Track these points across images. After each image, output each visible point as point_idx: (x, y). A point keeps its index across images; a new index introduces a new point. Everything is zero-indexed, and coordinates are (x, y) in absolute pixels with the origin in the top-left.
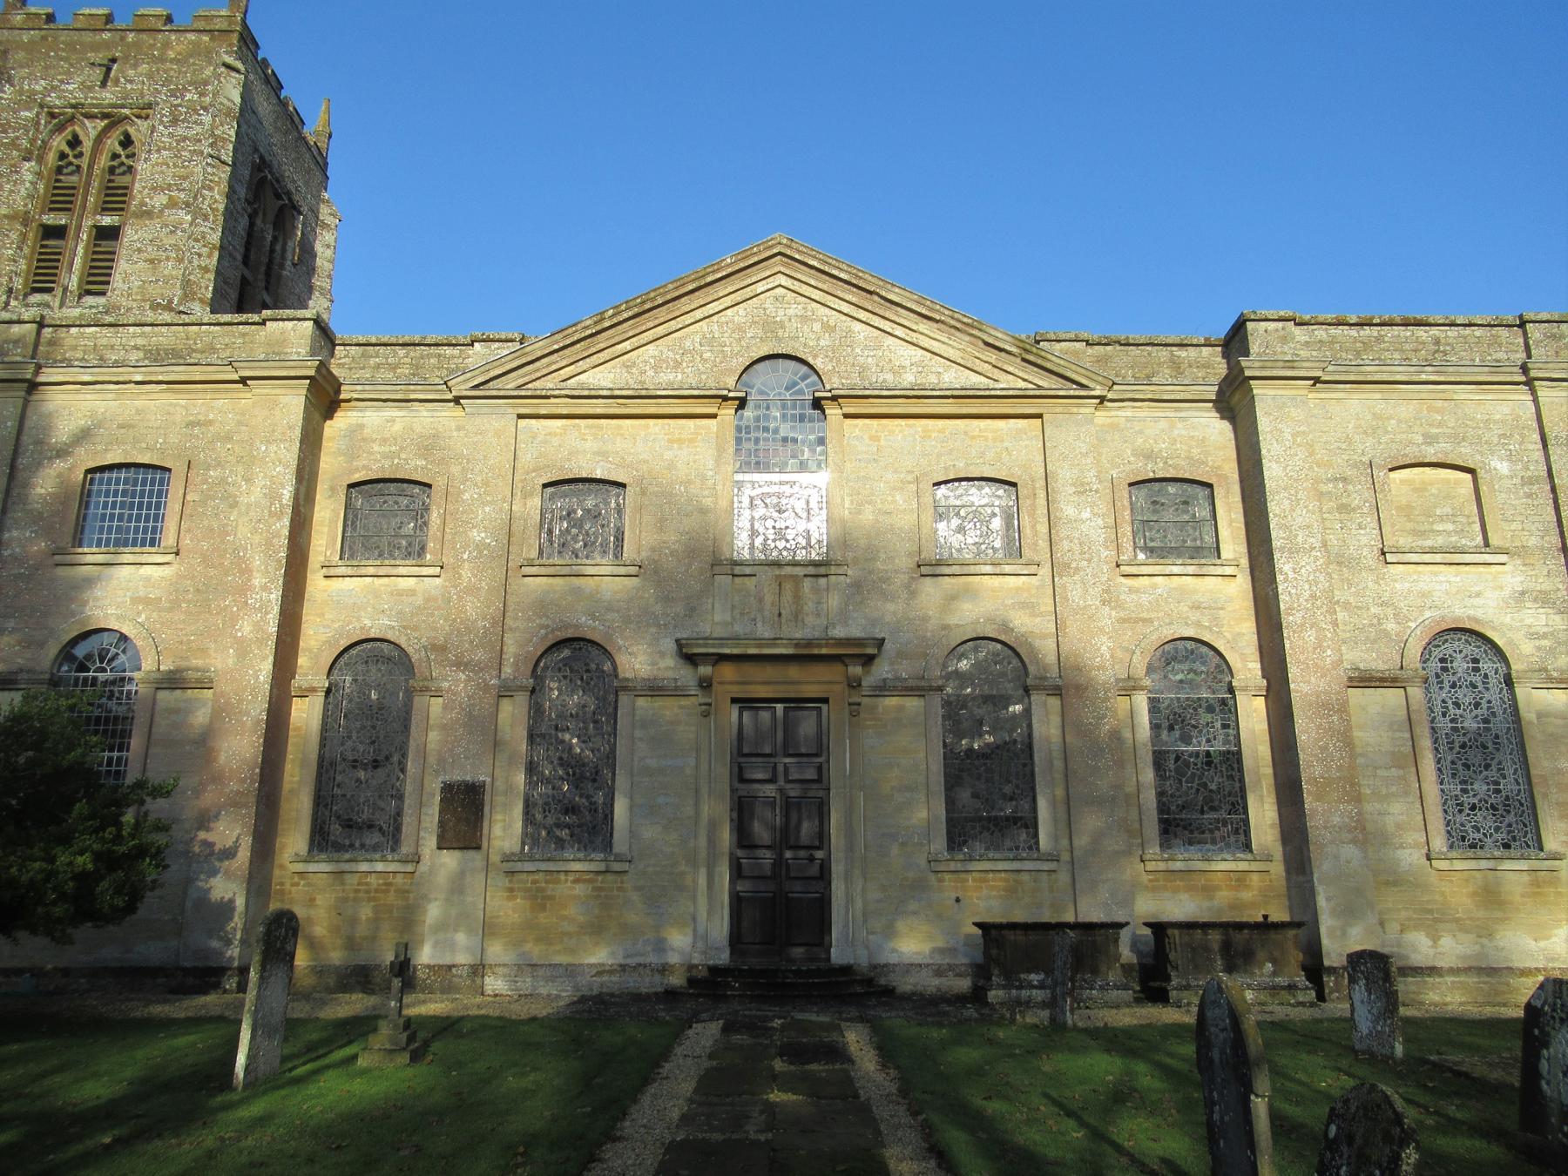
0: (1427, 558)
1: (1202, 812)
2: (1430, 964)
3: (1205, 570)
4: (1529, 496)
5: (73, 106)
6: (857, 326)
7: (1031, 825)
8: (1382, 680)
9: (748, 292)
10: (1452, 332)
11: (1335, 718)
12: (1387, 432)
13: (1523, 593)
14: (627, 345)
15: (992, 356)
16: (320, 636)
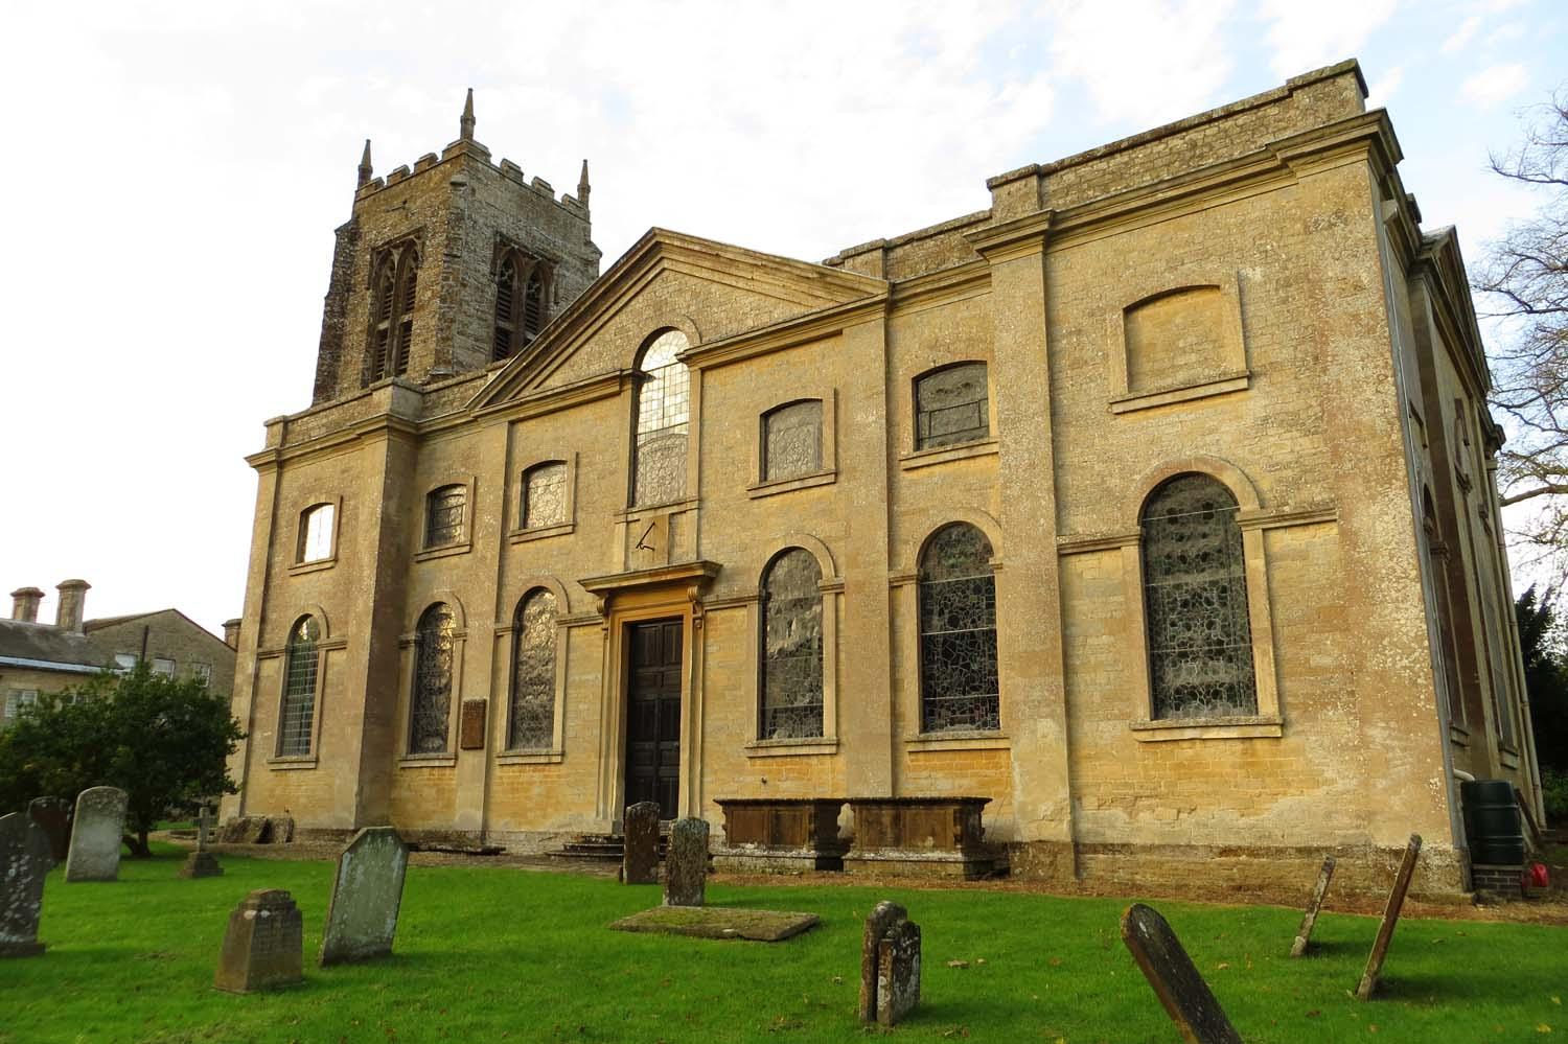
2: (1124, 841)
3: (975, 452)
4: (1285, 301)
5: (387, 243)
6: (714, 287)
8: (1095, 543)
10: (1211, 130)
11: (1042, 590)
12: (1128, 267)
13: (1266, 419)
14: (571, 350)
15: (804, 287)
16: (915, 532)
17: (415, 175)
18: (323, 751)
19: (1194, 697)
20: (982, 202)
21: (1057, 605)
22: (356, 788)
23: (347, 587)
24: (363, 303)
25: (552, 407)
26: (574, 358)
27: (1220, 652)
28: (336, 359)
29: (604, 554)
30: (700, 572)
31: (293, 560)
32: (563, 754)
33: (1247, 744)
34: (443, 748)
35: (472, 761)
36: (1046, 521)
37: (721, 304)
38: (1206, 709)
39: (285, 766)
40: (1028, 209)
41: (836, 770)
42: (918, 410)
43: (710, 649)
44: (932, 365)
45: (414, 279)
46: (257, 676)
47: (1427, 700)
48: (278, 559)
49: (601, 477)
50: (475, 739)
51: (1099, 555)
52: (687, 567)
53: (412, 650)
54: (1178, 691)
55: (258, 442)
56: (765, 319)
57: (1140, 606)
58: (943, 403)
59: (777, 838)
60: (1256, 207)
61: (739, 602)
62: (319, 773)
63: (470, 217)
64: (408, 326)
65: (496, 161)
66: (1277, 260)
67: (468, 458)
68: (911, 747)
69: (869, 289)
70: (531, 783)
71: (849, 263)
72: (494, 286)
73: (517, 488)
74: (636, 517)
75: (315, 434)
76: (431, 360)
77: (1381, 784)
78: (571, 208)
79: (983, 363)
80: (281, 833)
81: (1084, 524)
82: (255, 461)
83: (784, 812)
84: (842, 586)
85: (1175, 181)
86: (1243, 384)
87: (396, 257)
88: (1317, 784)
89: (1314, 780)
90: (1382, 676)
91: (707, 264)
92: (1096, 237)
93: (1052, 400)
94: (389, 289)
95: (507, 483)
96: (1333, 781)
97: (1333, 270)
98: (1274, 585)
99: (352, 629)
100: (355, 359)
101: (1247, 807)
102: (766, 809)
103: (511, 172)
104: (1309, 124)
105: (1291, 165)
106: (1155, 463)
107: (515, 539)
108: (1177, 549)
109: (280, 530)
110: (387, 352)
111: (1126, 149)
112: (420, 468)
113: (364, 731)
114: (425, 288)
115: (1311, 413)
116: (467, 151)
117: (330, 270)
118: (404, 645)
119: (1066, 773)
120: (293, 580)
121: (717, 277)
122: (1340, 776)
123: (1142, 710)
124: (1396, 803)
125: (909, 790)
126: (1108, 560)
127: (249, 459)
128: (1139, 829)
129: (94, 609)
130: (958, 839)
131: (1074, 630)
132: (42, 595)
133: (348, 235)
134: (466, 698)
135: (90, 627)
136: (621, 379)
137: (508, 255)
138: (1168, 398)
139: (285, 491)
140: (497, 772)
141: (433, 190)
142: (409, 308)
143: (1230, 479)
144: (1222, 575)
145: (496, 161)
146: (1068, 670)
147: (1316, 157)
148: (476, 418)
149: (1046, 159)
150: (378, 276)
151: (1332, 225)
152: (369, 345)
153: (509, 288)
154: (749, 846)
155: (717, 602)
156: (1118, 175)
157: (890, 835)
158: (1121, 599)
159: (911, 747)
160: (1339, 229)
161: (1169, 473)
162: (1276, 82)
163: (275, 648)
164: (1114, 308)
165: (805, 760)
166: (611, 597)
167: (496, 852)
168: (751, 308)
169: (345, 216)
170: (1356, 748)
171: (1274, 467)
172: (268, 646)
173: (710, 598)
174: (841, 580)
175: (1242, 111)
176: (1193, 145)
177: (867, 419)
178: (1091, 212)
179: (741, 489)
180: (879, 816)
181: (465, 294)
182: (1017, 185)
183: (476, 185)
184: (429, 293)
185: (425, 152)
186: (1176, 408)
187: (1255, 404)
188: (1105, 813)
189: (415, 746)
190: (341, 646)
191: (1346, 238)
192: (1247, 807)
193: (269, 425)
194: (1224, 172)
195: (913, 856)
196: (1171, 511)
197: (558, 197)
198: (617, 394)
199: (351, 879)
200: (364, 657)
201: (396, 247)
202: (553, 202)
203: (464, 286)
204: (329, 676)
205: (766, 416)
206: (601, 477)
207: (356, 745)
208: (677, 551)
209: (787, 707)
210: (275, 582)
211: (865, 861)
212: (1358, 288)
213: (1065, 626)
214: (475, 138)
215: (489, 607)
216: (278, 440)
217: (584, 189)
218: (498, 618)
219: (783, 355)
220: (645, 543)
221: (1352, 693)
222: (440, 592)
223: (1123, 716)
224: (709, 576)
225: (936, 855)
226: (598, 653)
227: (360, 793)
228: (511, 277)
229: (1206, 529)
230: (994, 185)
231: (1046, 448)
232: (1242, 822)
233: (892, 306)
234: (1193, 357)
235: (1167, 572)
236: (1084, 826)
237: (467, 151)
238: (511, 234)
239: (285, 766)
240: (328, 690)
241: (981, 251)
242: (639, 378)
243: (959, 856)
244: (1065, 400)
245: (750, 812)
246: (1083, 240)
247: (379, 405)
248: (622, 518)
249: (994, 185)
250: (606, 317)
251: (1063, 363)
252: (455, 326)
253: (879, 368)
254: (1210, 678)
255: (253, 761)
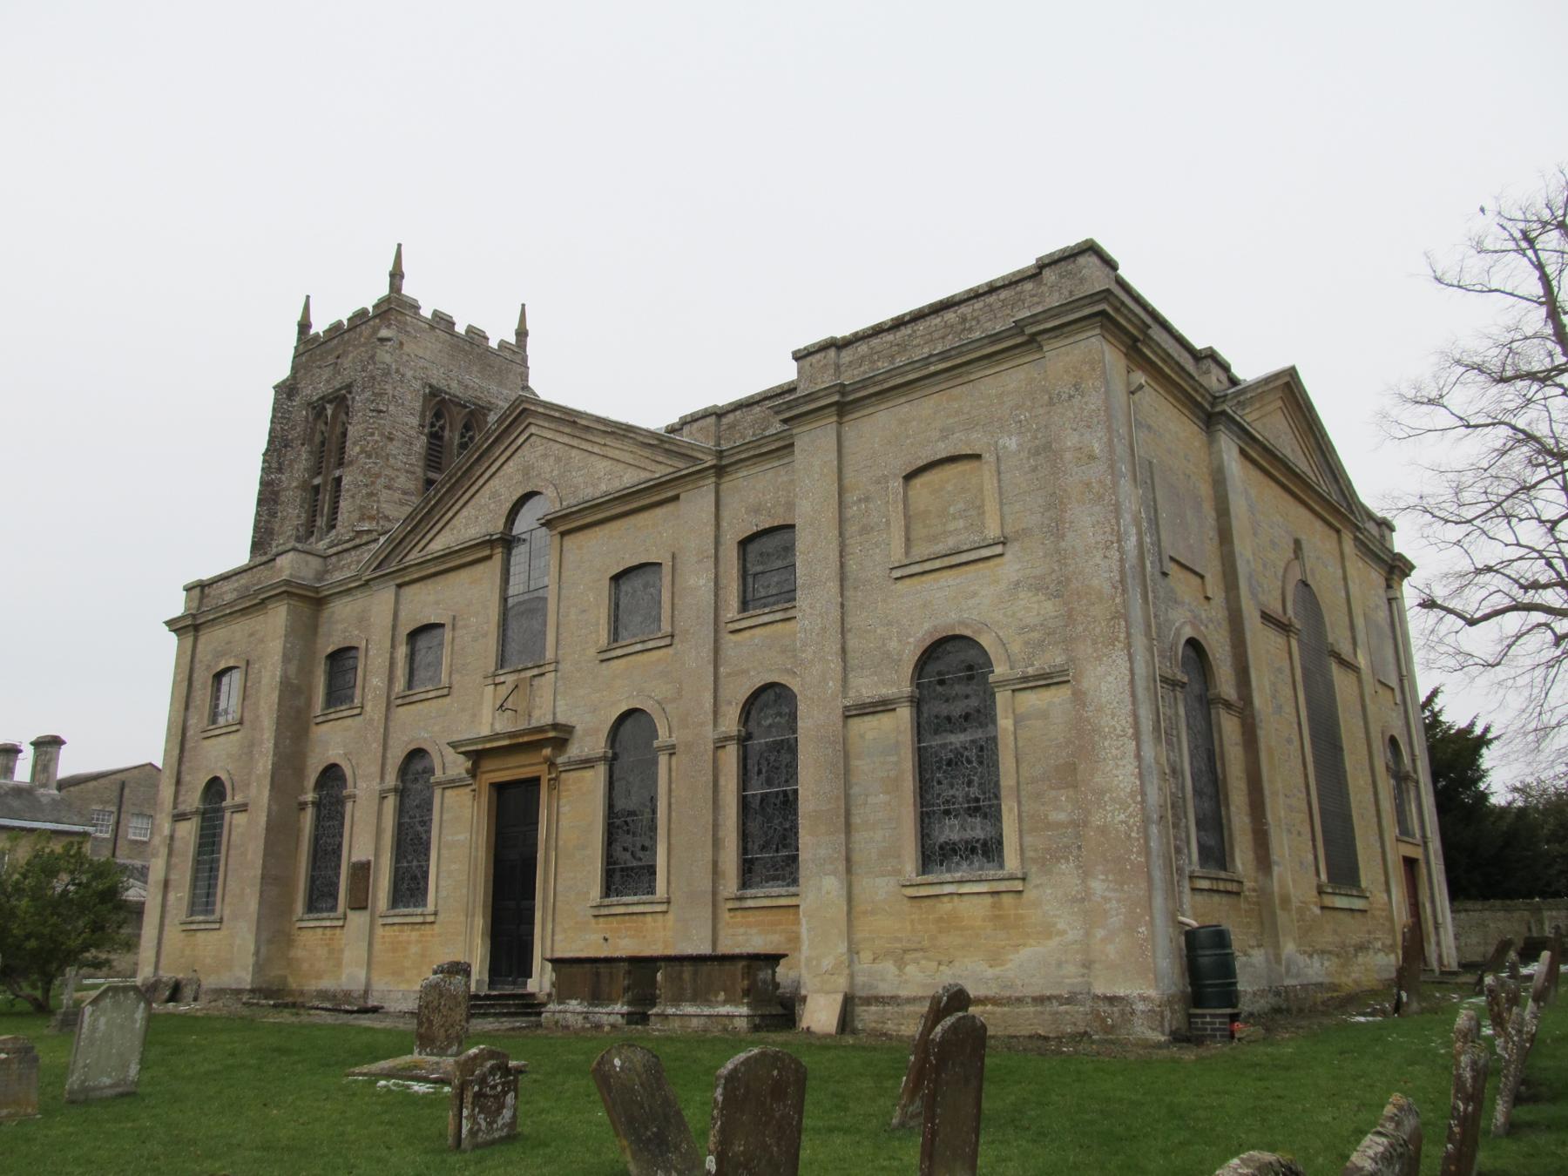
0: (928, 566)
1: (777, 851)
6: (574, 453)
7: (652, 870)
9: (514, 447)
10: (978, 305)
12: (908, 437)
13: (1017, 584)
14: (450, 514)
15: (647, 453)
17: (349, 330)
18: (227, 913)
19: (955, 852)
20: (787, 372)
21: (841, 765)
22: (252, 948)
23: (250, 748)
24: (302, 459)
25: (433, 570)
26: (454, 521)
27: (977, 809)
28: (273, 515)
29: (474, 715)
30: (551, 734)
31: (206, 721)
32: (435, 914)
33: (996, 898)
34: (334, 908)
35: (358, 919)
36: (833, 685)
37: (580, 469)
38: (965, 865)
39: (194, 927)
40: (826, 380)
41: (667, 927)
42: (744, 574)
43: (563, 810)
44: (755, 529)
45: (344, 434)
46: (172, 837)
47: (1139, 853)
48: (192, 722)
49: (475, 640)
50: (360, 902)
51: (880, 716)
52: (540, 729)
53: (310, 811)
54: (941, 848)
55: (177, 606)
56: (617, 485)
57: (910, 765)
58: (764, 564)
59: (597, 997)
60: (1013, 378)
61: (587, 763)
62: (221, 933)
63: (397, 371)
64: (339, 480)
65: (426, 312)
66: (1029, 430)
67: (362, 620)
68: (730, 905)
69: (700, 456)
70: (409, 943)
71: (686, 429)
72: (424, 438)
73: (402, 650)
74: (502, 679)
75: (228, 597)
76: (356, 515)
77: (1100, 933)
78: (507, 354)
79: (792, 527)
80: (188, 992)
81: (866, 687)
82: (171, 624)
83: (603, 969)
84: (673, 747)
85: (944, 356)
86: (998, 549)
87: (329, 412)
88: (1049, 936)
89: (1048, 931)
90: (1103, 831)
91: (567, 430)
92: (883, 407)
93: (842, 565)
94: (323, 443)
95: (393, 646)
96: (1064, 932)
97: (1071, 440)
98: (1020, 744)
99: (253, 791)
100: (292, 514)
101: (995, 959)
102: (588, 966)
103: (442, 322)
104: (1054, 301)
105: (1039, 338)
106: (926, 626)
107: (399, 701)
108: (944, 709)
109: (199, 692)
110: (320, 503)
111: (909, 322)
112: (321, 630)
113: (261, 893)
114: (354, 444)
115: (1054, 576)
116: (395, 307)
117: (268, 425)
118: (302, 806)
119: (844, 928)
120: (207, 743)
121: (575, 442)
122: (1069, 926)
123: (910, 866)
124: (1111, 951)
125: (725, 948)
126: (885, 721)
127: (169, 623)
128: (906, 982)
129: (68, 765)
130: (747, 993)
131: (855, 790)
132: (63, 743)
133: (286, 391)
134: (354, 859)
135: (63, 785)
136: (490, 543)
137: (438, 405)
138: (938, 564)
139: (199, 656)
140: (380, 931)
141: (364, 345)
142: (340, 464)
143: (985, 641)
144: (979, 734)
145: (426, 312)
146: (848, 827)
147: (1058, 332)
148: (367, 582)
149: (843, 331)
150: (313, 431)
151: (1071, 397)
152: (303, 501)
153: (441, 438)
154: (574, 1002)
155: (569, 763)
156: (903, 347)
157: (689, 992)
158: (894, 759)
159: (730, 905)
160: (1075, 401)
161: (937, 636)
162: (1027, 261)
163: (188, 809)
164: (895, 476)
165: (641, 918)
166: (478, 757)
167: (375, 1010)
168: (607, 475)
169: (284, 371)
170: (1083, 900)
171: (1023, 629)
172: (182, 808)
173: (560, 760)
174: (674, 740)
175: (1004, 287)
176: (964, 320)
177: (697, 581)
178: (875, 384)
179: (592, 651)
180: (681, 972)
181: (392, 448)
182: (818, 356)
183: (404, 338)
184: (357, 449)
185: (334, 320)
186: (945, 573)
187: (1010, 568)
188: (878, 966)
189: (311, 907)
190: (242, 808)
191: (1082, 409)
192: (995, 959)
193: (188, 589)
194: (981, 348)
195: (707, 1011)
196: (939, 673)
197: (493, 343)
198: (489, 557)
199: (94, 1029)
200: (263, 820)
201: (330, 402)
202: (488, 349)
203: (391, 440)
204: (233, 837)
205: (617, 579)
206: (475, 640)
207: (253, 906)
208: (536, 713)
209: (626, 871)
210: (189, 745)
211: (667, 1016)
212: (1092, 457)
213: (847, 785)
214: (404, 292)
215: (375, 769)
216: (195, 604)
217: (522, 333)
218: (382, 778)
219: (632, 520)
220: (509, 704)
221: (1079, 847)
222: (334, 754)
223: (898, 872)
224: (560, 736)
225: (723, 1010)
226: (467, 813)
227: (257, 952)
228: (442, 428)
229: (968, 690)
230: (799, 356)
231: (835, 613)
232: (990, 972)
233: (720, 471)
234: (961, 523)
235: (936, 732)
236: (860, 980)
237: (395, 307)
238: (442, 384)
239: (194, 927)
240: (232, 852)
241: (785, 421)
242: (507, 542)
243: (744, 1010)
244: (852, 565)
245: (576, 969)
246: (871, 410)
247: (281, 570)
248: (490, 681)
249: (799, 356)
250: (481, 481)
251: (852, 529)
252: (383, 480)
253: (710, 530)
254: (969, 835)
255: (167, 921)
